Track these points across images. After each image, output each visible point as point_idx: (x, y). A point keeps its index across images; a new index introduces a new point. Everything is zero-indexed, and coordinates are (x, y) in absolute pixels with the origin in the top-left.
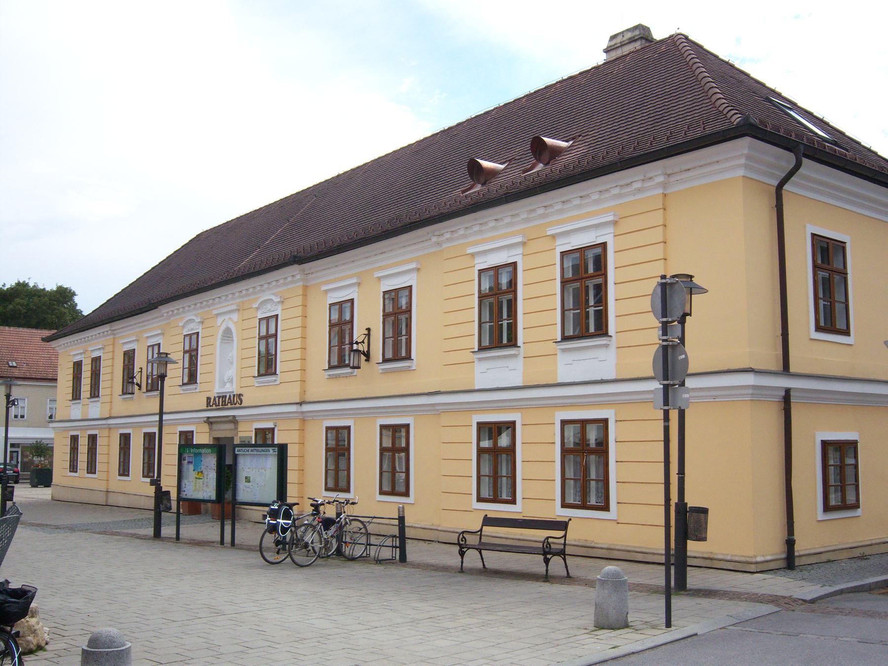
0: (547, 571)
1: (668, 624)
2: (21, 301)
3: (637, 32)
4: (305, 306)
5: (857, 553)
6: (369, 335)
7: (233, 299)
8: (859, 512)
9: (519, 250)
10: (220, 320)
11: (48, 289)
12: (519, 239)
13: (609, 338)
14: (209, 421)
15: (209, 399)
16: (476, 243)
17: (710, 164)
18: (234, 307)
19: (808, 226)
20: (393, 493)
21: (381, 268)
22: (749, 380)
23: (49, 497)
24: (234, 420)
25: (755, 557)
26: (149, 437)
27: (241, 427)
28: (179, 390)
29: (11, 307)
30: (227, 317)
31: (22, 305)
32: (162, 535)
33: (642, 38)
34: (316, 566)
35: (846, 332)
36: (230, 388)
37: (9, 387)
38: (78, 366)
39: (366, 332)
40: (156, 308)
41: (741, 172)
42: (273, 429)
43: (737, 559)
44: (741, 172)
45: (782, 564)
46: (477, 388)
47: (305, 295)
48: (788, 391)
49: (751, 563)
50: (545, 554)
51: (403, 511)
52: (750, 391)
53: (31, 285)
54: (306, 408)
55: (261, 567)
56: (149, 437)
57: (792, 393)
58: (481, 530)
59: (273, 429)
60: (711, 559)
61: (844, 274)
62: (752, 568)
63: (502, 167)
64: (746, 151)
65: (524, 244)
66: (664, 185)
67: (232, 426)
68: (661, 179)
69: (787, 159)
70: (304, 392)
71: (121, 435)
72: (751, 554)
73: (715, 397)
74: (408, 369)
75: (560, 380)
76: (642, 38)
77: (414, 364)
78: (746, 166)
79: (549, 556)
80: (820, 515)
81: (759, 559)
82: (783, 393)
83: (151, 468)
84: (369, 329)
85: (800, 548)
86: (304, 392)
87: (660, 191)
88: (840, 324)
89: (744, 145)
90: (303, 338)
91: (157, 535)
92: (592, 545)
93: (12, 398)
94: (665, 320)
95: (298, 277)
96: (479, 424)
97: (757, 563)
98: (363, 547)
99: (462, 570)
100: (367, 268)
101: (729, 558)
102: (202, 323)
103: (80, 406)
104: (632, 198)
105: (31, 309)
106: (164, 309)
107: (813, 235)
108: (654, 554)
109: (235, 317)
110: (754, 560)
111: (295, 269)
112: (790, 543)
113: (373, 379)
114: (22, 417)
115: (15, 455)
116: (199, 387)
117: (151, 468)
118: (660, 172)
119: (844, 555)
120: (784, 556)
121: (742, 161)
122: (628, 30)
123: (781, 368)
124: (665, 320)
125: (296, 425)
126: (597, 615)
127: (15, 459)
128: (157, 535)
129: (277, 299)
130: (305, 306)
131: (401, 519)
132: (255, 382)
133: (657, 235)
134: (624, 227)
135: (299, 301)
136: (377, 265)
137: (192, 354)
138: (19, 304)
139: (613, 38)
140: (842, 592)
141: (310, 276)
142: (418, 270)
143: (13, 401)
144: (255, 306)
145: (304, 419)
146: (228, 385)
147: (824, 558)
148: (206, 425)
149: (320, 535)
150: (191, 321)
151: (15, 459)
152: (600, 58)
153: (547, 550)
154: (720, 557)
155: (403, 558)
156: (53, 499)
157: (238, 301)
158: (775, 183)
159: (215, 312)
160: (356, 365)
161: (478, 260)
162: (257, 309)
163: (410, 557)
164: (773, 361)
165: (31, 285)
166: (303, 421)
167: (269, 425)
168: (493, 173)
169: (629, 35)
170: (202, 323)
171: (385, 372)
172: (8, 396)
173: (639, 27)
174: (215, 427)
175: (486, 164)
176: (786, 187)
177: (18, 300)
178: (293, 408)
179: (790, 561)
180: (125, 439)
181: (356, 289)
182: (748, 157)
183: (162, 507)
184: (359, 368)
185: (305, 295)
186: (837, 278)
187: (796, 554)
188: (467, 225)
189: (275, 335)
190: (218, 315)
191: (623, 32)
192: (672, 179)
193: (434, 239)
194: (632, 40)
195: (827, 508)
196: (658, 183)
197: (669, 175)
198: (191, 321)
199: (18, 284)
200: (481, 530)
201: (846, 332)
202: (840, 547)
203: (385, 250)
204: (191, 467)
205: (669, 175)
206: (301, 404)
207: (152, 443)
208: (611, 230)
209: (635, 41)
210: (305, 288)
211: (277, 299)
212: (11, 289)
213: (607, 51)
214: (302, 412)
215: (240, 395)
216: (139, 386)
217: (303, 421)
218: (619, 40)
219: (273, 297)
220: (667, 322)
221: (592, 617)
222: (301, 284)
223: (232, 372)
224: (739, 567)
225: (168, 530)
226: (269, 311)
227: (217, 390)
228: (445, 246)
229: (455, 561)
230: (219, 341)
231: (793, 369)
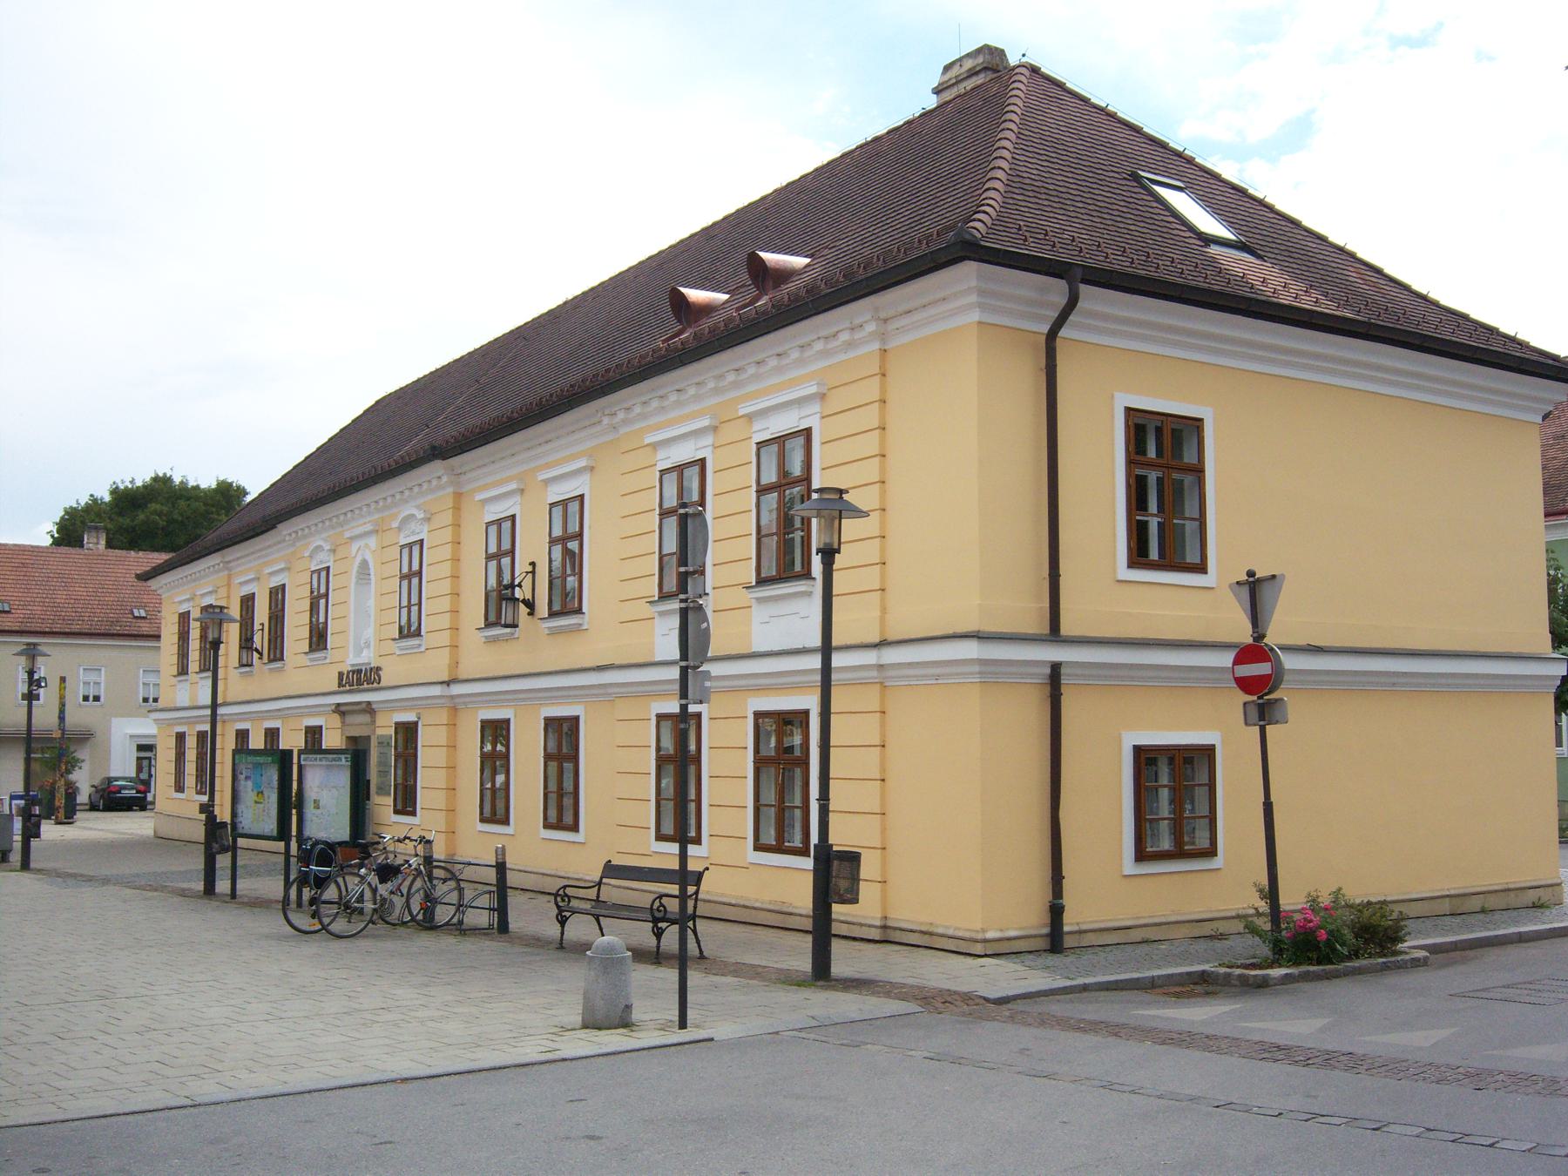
0: (658, 947)
1: (683, 1024)
2: (158, 507)
3: (980, 59)
4: (457, 525)
5: (1207, 929)
6: (533, 572)
7: (370, 513)
8: (1217, 862)
9: (708, 440)
10: (355, 546)
11: (203, 486)
12: (706, 422)
13: (810, 582)
14: (340, 710)
15: (341, 674)
16: (658, 427)
17: (936, 302)
18: (369, 527)
19: (1117, 395)
20: (558, 826)
21: (548, 466)
22: (970, 650)
23: (151, 832)
24: (369, 709)
25: (984, 931)
26: (201, 736)
27: (381, 720)
28: (305, 660)
29: (142, 517)
30: (362, 543)
31: (160, 514)
32: (217, 890)
33: (986, 69)
34: (366, 937)
35: (1201, 568)
36: (367, 658)
37: (31, 653)
38: (184, 618)
39: (530, 569)
40: (273, 527)
41: (975, 316)
42: (416, 724)
43: (960, 934)
44: (975, 316)
45: (1042, 944)
46: (658, 659)
47: (457, 509)
48: (1056, 668)
49: (976, 941)
50: (655, 921)
51: (504, 854)
52: (976, 668)
53: (177, 480)
54: (457, 689)
55: (281, 938)
56: (201, 736)
57: (1063, 671)
58: (600, 884)
59: (416, 724)
60: (931, 934)
61: (1198, 471)
62: (978, 949)
63: (726, 297)
64: (974, 283)
65: (715, 429)
66: (883, 336)
67: (366, 718)
68: (871, 327)
69: (1056, 292)
70: (455, 664)
71: (550, 722)
72: (978, 926)
73: (938, 677)
74: (578, 629)
75: (756, 648)
76: (986, 69)
77: (585, 620)
78: (982, 307)
79: (662, 925)
80: (1129, 866)
81: (990, 935)
82: (1048, 671)
83: (206, 780)
84: (533, 564)
85: (1070, 923)
86: (455, 664)
87: (876, 346)
88: (1192, 557)
89: (968, 273)
90: (455, 577)
91: (209, 890)
92: (790, 910)
93: (36, 677)
94: (682, 569)
95: (445, 479)
96: (546, 719)
97: (985, 941)
98: (452, 909)
99: (561, 946)
100: (532, 465)
101: (950, 932)
102: (334, 551)
103: (187, 685)
104: (843, 357)
105: (175, 521)
106: (285, 529)
107: (1128, 410)
108: (861, 925)
109: (372, 542)
110: (980, 936)
111: (436, 468)
112: (1056, 912)
113: (536, 643)
114: (97, 699)
115: (145, 763)
116: (330, 655)
117: (206, 780)
118: (868, 317)
119: (1185, 931)
120: (1046, 930)
121: (973, 298)
122: (968, 55)
123: (1047, 631)
124: (682, 569)
125: (443, 717)
126: (585, 1009)
127: (145, 769)
128: (209, 890)
129: (420, 515)
130: (457, 525)
131: (501, 868)
132: (394, 647)
133: (870, 417)
134: (834, 404)
135: (447, 518)
136: (541, 462)
137: (318, 600)
138: (155, 512)
139: (947, 68)
140: (1085, 988)
141: (463, 478)
142: (592, 469)
143: (39, 681)
144: (395, 525)
145: (454, 708)
146: (365, 652)
147: (1136, 935)
148: (337, 717)
149: (374, 891)
150: (319, 548)
151: (145, 769)
152: (932, 102)
153: (658, 915)
154: (940, 931)
155: (503, 927)
156: (157, 836)
157: (376, 516)
158: (1045, 328)
159: (347, 535)
160: (509, 621)
161: (661, 454)
162: (399, 529)
163: (514, 923)
164: (1032, 618)
165: (177, 480)
166: (454, 710)
167: (409, 717)
168: (707, 309)
169: (969, 64)
170: (334, 551)
171: (554, 632)
172: (31, 673)
173: (987, 50)
174: (350, 719)
175: (695, 295)
176: (1063, 333)
177: (153, 506)
178: (436, 691)
179: (1055, 940)
180: (496, 731)
181: (518, 498)
182: (982, 293)
183: (216, 846)
184: (516, 626)
185: (457, 509)
186: (1188, 479)
187: (1066, 929)
188: (644, 399)
189: (420, 573)
190: (352, 538)
191: (960, 59)
192: (892, 326)
193: (606, 421)
194: (973, 73)
195: (1141, 856)
196: (871, 334)
197: (885, 321)
198: (319, 548)
199: (156, 479)
200: (600, 884)
201: (1201, 568)
202: (1173, 919)
203: (549, 437)
204: (249, 783)
205: (885, 321)
206: (448, 683)
207: (207, 742)
208: (816, 407)
209: (977, 73)
210: (458, 496)
211: (420, 515)
212: (145, 487)
213: (937, 91)
214: (452, 697)
215: (379, 669)
216: (261, 654)
217: (454, 710)
218: (955, 71)
219: (415, 512)
220: (686, 574)
221: (580, 1009)
222: (450, 490)
223: (370, 633)
224: (963, 947)
225: (222, 886)
226: (413, 533)
227: (354, 659)
228: (623, 431)
229: (553, 930)
230: (354, 580)
231: (1066, 629)
